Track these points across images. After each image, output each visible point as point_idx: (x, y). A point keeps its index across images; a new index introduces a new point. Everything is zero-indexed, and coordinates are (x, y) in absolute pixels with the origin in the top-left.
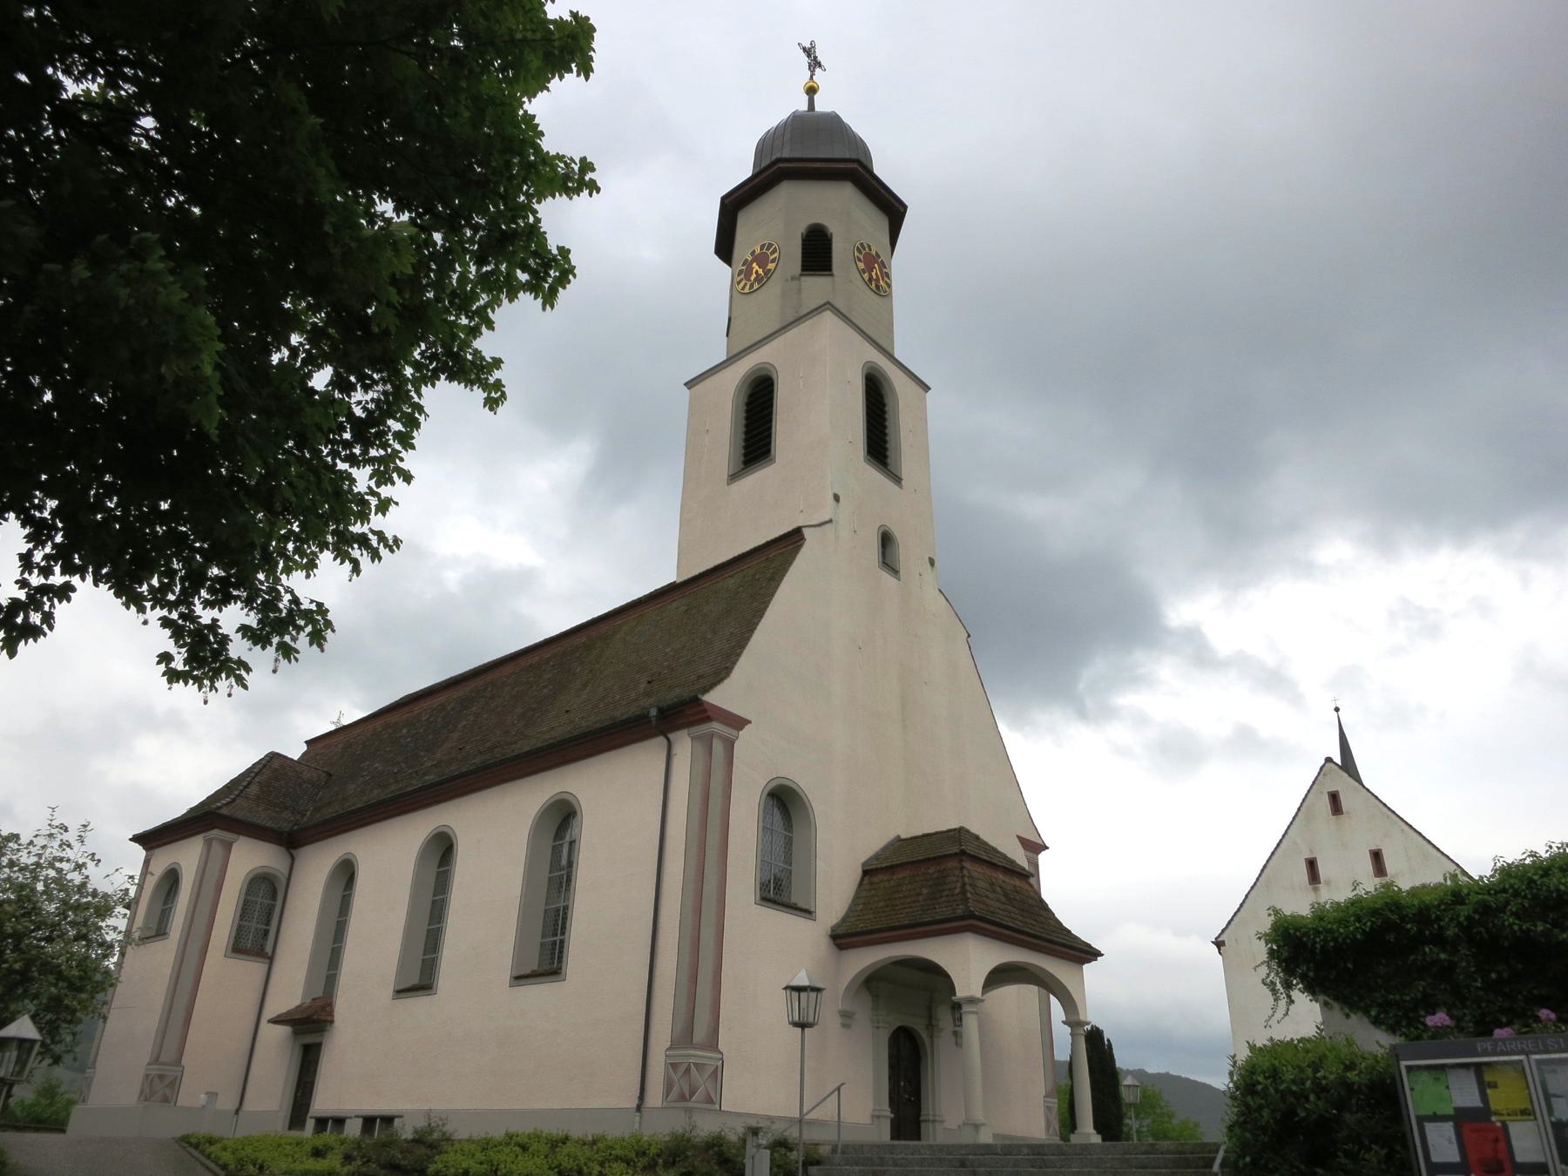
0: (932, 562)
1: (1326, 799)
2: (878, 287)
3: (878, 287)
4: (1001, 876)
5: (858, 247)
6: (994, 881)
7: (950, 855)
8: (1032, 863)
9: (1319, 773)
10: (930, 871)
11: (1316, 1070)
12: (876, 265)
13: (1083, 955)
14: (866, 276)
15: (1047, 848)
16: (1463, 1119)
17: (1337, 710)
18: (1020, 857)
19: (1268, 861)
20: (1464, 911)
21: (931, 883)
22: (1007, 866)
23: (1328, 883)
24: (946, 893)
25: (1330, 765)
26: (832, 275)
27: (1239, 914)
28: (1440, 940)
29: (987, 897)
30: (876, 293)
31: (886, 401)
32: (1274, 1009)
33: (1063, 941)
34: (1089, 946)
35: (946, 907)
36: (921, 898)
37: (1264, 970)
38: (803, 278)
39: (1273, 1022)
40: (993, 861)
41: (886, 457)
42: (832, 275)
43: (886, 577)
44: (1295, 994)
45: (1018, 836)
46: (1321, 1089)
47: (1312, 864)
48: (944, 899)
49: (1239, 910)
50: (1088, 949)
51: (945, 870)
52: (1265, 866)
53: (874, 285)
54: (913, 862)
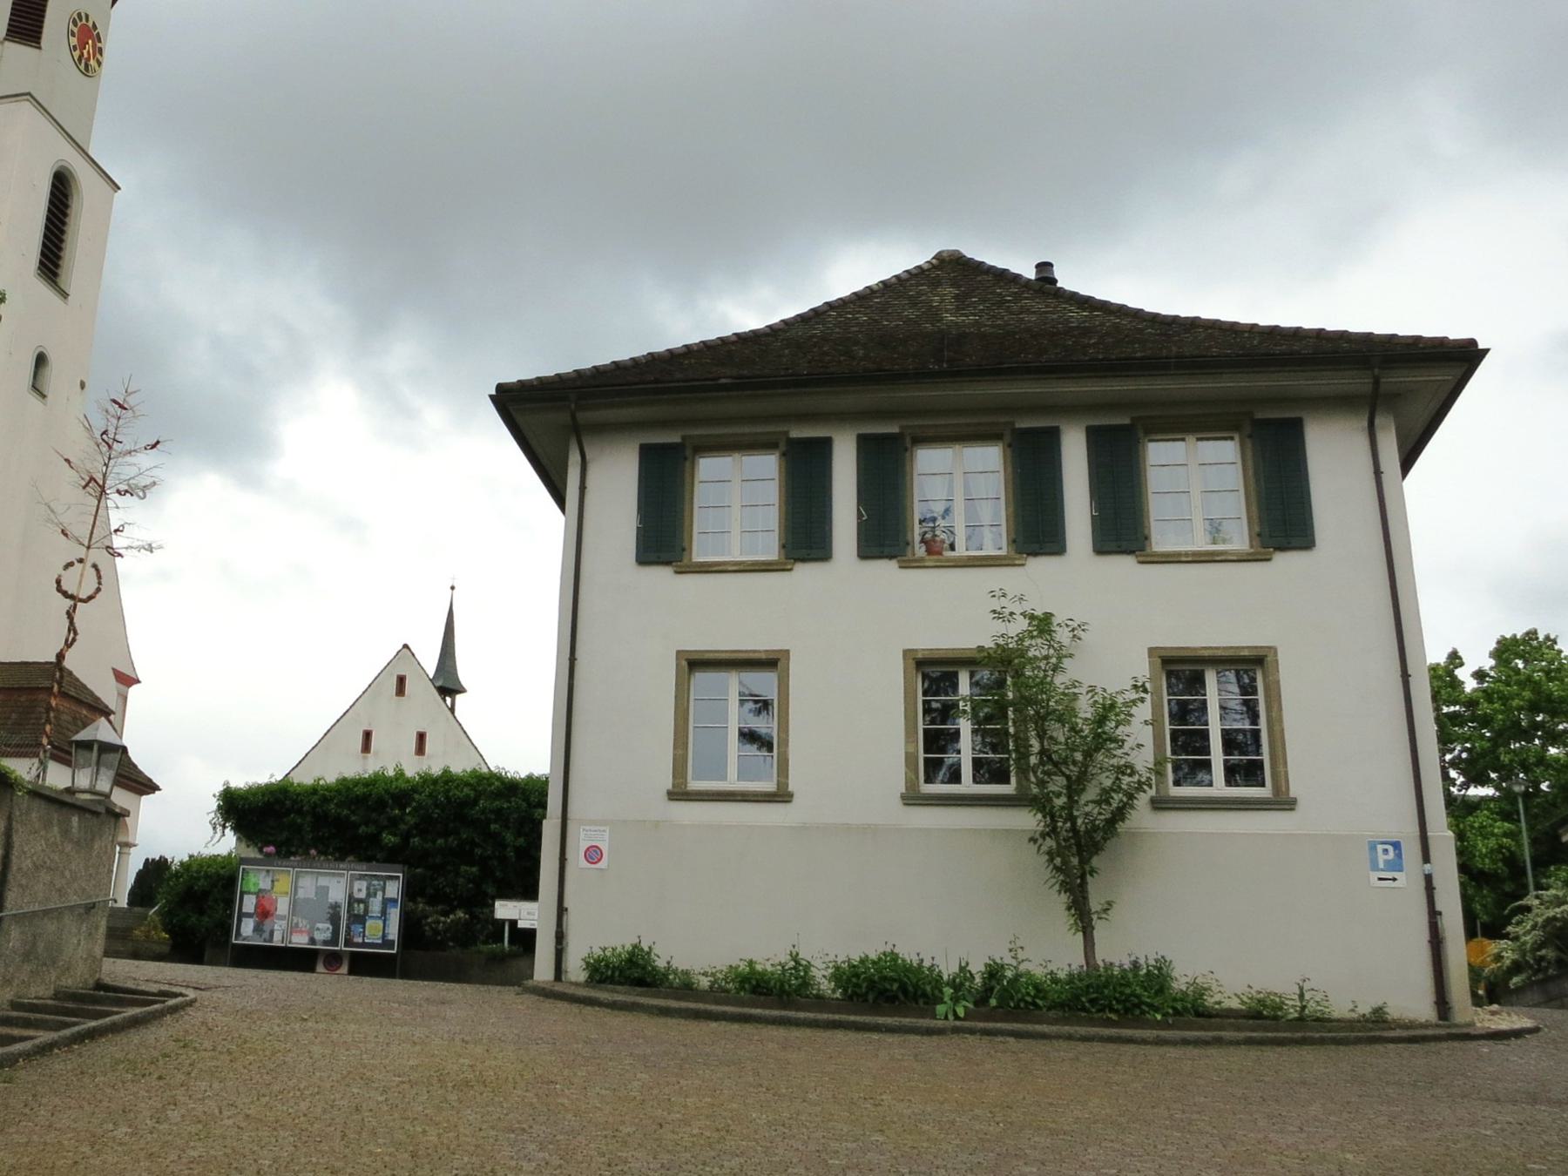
0: (83, 385)
1: (394, 681)
2: (87, 66)
3: (87, 66)
4: (85, 712)
5: (74, 19)
6: (77, 715)
7: (42, 688)
8: (122, 695)
9: (395, 657)
10: (22, 699)
11: (208, 867)
12: (90, 42)
13: (142, 788)
14: (76, 54)
15: (138, 682)
16: (260, 894)
17: (453, 588)
18: (105, 690)
19: (332, 727)
20: (315, 798)
21: (21, 710)
22: (92, 703)
23: (376, 754)
24: (33, 721)
25: (405, 650)
26: (40, 48)
27: (296, 770)
28: (300, 812)
29: (68, 730)
30: (83, 73)
31: (70, 203)
32: (212, 838)
33: (126, 774)
34: (150, 780)
35: (31, 734)
36: (10, 722)
37: (213, 815)
38: (7, 43)
39: (209, 845)
40: (81, 698)
41: (56, 275)
42: (40, 48)
43: (33, 400)
44: (228, 831)
45: (114, 670)
46: (207, 876)
47: (367, 735)
48: (30, 727)
49: (297, 765)
50: (149, 783)
51: (35, 700)
52: (329, 731)
53: (83, 64)
54: (9, 689)
